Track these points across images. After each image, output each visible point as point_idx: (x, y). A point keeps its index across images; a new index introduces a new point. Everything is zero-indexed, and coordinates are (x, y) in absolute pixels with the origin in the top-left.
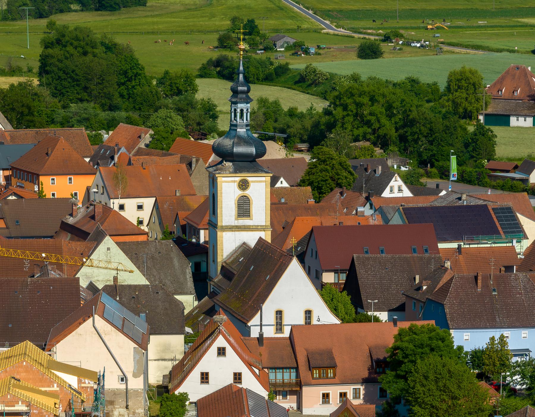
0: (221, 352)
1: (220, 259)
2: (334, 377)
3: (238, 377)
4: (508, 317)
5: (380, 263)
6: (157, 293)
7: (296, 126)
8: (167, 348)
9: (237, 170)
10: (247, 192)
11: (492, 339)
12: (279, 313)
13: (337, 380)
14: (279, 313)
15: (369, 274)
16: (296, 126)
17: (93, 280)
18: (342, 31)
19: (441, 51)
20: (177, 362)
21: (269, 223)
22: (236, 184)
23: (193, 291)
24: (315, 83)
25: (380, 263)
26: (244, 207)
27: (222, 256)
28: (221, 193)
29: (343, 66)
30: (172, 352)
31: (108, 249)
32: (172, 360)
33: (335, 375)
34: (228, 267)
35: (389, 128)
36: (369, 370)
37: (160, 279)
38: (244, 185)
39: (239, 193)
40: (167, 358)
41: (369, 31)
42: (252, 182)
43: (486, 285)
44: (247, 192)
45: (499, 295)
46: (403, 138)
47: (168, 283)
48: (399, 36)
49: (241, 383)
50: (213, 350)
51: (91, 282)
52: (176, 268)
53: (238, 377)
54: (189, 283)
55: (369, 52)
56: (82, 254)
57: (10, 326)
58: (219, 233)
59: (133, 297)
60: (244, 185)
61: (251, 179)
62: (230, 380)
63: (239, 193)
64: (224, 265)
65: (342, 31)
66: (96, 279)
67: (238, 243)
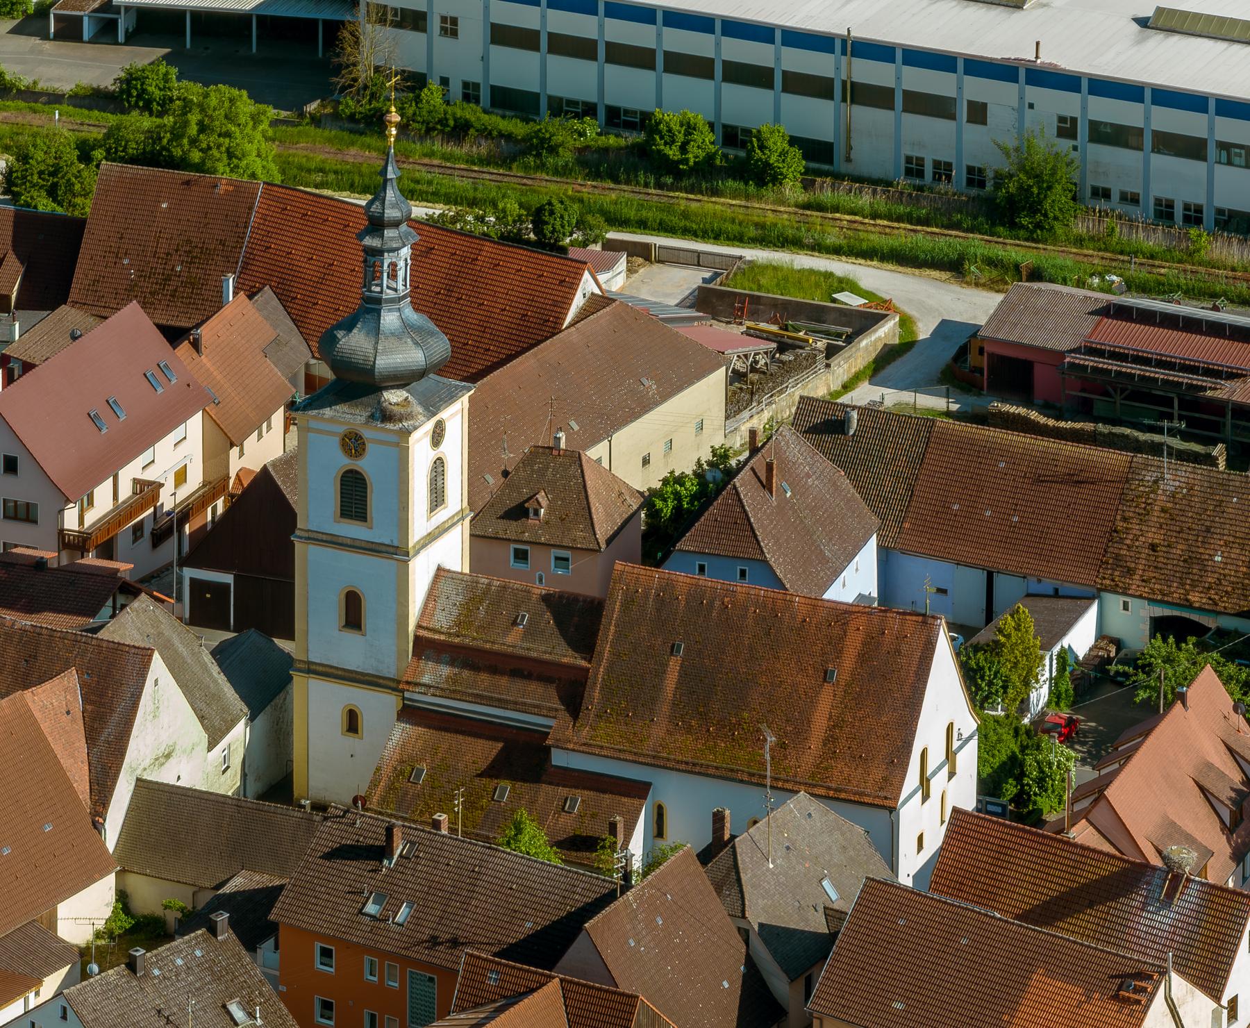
6: (810, 815)
34: (457, 640)
56: (68, 713)
59: (788, 848)
64: (422, 633)
66: (141, 767)
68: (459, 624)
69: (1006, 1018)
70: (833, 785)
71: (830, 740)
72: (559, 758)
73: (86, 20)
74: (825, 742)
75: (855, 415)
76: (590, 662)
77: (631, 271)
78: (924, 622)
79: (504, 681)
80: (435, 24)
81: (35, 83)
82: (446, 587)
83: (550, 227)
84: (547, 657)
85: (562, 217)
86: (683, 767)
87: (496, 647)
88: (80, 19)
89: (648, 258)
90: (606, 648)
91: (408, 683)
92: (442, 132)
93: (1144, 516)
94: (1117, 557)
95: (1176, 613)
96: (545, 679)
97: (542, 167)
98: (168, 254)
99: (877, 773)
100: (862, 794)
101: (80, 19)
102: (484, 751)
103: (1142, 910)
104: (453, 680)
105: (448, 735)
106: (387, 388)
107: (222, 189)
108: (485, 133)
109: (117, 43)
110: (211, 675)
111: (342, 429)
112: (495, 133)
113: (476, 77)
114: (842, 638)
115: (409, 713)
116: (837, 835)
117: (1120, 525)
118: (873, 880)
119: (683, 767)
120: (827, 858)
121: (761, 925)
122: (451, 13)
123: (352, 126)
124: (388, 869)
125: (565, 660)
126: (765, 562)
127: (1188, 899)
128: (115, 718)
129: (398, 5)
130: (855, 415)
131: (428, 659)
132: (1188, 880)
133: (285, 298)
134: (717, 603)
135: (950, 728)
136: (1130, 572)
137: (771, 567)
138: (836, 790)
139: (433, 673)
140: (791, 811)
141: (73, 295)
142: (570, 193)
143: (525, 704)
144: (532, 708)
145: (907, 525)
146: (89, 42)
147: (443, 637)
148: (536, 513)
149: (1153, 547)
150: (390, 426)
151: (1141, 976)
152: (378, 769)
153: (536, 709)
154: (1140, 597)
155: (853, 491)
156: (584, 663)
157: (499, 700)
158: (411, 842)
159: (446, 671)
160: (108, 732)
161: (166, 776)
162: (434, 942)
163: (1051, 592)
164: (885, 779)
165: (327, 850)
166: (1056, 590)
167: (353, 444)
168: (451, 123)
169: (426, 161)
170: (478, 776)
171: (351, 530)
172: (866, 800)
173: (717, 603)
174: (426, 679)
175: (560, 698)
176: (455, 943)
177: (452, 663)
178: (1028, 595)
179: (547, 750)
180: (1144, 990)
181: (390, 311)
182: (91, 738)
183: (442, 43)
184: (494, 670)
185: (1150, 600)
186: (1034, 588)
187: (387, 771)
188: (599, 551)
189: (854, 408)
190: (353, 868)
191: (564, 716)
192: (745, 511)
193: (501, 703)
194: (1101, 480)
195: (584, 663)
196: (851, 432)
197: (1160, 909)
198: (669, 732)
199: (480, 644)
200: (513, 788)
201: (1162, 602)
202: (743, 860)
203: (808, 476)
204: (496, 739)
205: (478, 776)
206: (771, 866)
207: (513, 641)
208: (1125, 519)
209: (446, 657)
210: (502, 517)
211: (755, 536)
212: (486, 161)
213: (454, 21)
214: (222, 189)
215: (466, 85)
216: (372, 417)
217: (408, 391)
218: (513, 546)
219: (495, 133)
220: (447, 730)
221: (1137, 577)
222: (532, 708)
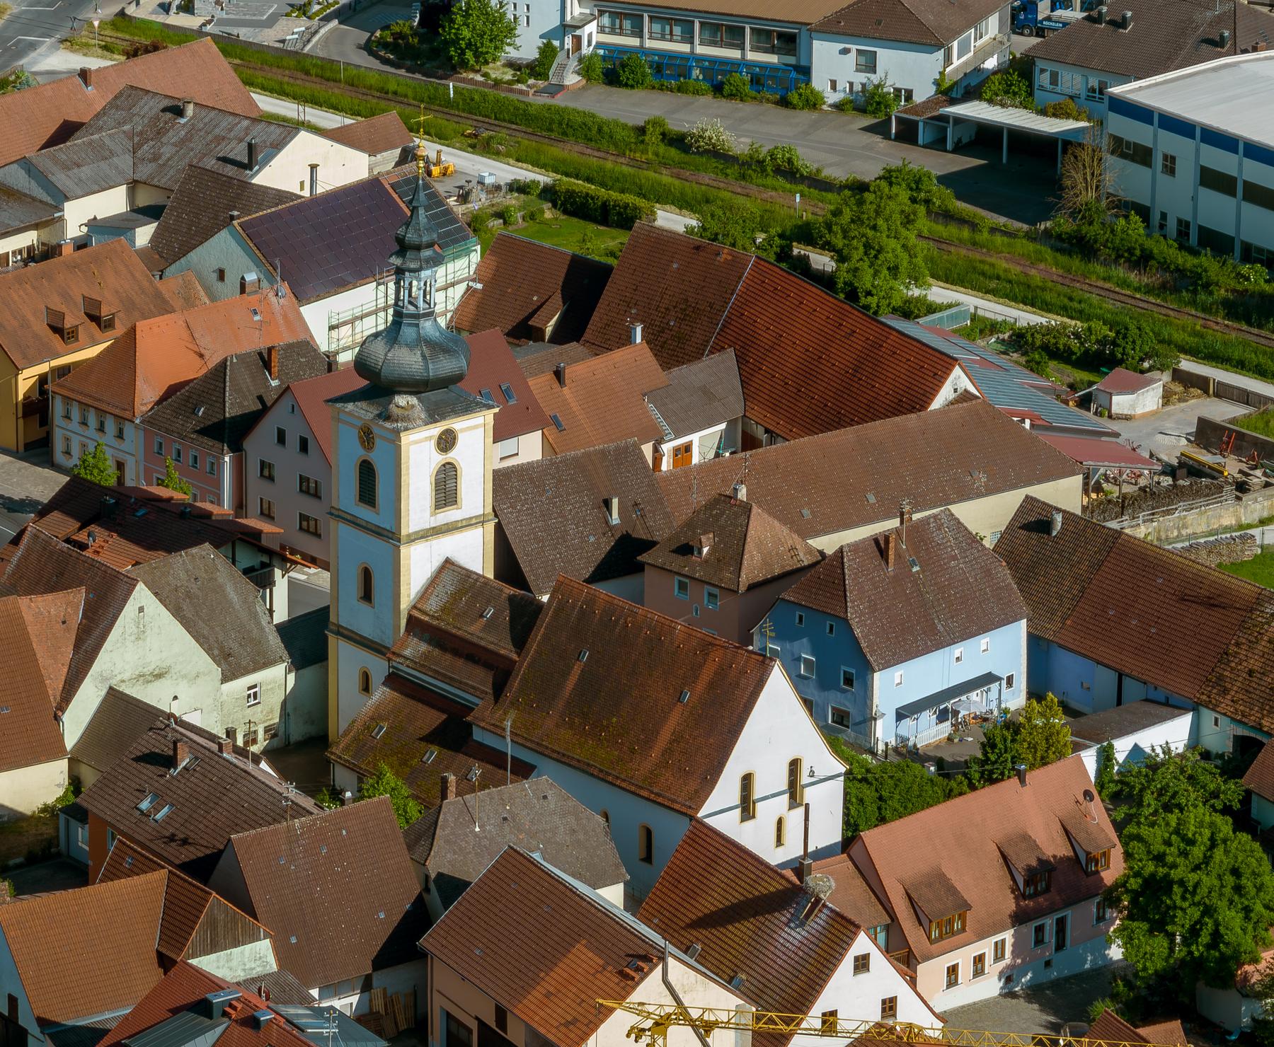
0: (862, 964)
1: (405, 604)
2: (963, 929)
3: (889, 1006)
4: (952, 617)
5: (531, 479)
6: (545, 797)
10: (452, 456)
12: (747, 781)
13: (969, 933)
14: (747, 781)
15: (519, 511)
17: (113, 682)
21: (489, 509)
22: (433, 443)
23: (285, 655)
25: (531, 479)
26: (446, 488)
27: (409, 596)
28: (408, 468)
31: (141, 609)
34: (435, 623)
36: (1013, 892)
37: (217, 641)
38: (447, 442)
39: (438, 459)
42: (463, 430)
45: (923, 571)
49: (894, 1016)
50: (847, 963)
51: (111, 688)
52: (237, 607)
53: (889, 1006)
54: (271, 637)
56: (64, 622)
57: (294, 940)
59: (505, 819)
60: (447, 442)
61: (457, 424)
62: (876, 1016)
63: (438, 459)
64: (416, 614)
66: (119, 678)
67: (437, 563)
68: (443, 610)
69: (542, 975)
70: (656, 790)
71: (667, 752)
72: (478, 735)
73: (921, 125)
74: (664, 752)
75: (1059, 518)
76: (519, 655)
77: (1167, 398)
78: (763, 662)
79: (460, 662)
80: (1158, 161)
81: (818, 171)
82: (447, 577)
83: (1121, 350)
84: (492, 647)
85: (1134, 342)
86: (555, 755)
87: (459, 633)
88: (916, 123)
89: (1206, 392)
90: (533, 646)
91: (394, 653)
92: (1128, 260)
93: (1252, 644)
94: (1221, 678)
95: (1253, 735)
96: (488, 666)
97: (1193, 303)
98: (667, 309)
99: (693, 785)
100: (673, 801)
101: (916, 123)
102: (432, 719)
103: (787, 925)
104: (426, 656)
105: (412, 702)
106: (400, 393)
107: (722, 258)
108: (1164, 266)
109: (946, 151)
110: (258, 623)
111: (359, 424)
112: (1172, 267)
113: (1187, 217)
114: (701, 666)
115: (394, 680)
116: (571, 819)
117: (1233, 649)
118: (515, 851)
119: (555, 755)
120: (548, 835)
121: (440, 875)
122: (1171, 152)
123: (1059, 244)
124: (172, 776)
125: (502, 652)
126: (846, 620)
127: (821, 919)
128: (97, 632)
129: (1132, 140)
130: (1059, 518)
131: (415, 636)
132: (824, 906)
133: (741, 360)
134: (622, 621)
135: (795, 765)
136: (1225, 691)
137: (850, 626)
138: (657, 794)
139: (415, 648)
140: (525, 790)
141: (588, 335)
142: (1198, 327)
143: (467, 684)
144: (470, 685)
145: (1068, 622)
146: (924, 146)
147: (427, 619)
148: (700, 552)
149: (1251, 673)
150: (388, 425)
151: (646, 959)
152: (354, 722)
153: (474, 690)
154: (1225, 714)
155: (1010, 580)
156: (515, 657)
157: (451, 678)
158: (197, 758)
159: (423, 647)
160: (90, 642)
161: (156, 696)
162: (172, 838)
163: (1163, 700)
164: (696, 791)
165: (139, 754)
166: (1167, 699)
167: (367, 437)
168: (1138, 252)
169: (1100, 283)
170: (421, 739)
171: (364, 513)
172: (677, 807)
173: (622, 621)
174: (407, 652)
175: (494, 684)
176: (185, 842)
177: (429, 642)
178: (1146, 700)
179: (469, 726)
180: (642, 970)
181: (410, 325)
182: (77, 647)
183: (1163, 179)
184: (456, 653)
185: (1233, 719)
186: (1153, 695)
187: (358, 725)
188: (737, 592)
189: (1058, 510)
190: (149, 770)
191: (491, 698)
192: (844, 574)
193: (450, 681)
194: (1231, 606)
195: (515, 657)
196: (1054, 534)
197: (797, 926)
198: (557, 726)
199: (449, 628)
200: (439, 753)
201: (1240, 722)
202: (446, 820)
203: (954, 558)
204: (442, 710)
205: (421, 739)
206: (477, 829)
207: (473, 631)
208: (1238, 644)
209: (427, 635)
210: (673, 551)
211: (845, 596)
212: (1149, 290)
213: (1173, 159)
214: (722, 258)
215: (1180, 221)
216: (379, 416)
217: (419, 399)
218: (677, 578)
219: (1172, 267)
220: (413, 698)
221: (1229, 697)
222: (470, 685)
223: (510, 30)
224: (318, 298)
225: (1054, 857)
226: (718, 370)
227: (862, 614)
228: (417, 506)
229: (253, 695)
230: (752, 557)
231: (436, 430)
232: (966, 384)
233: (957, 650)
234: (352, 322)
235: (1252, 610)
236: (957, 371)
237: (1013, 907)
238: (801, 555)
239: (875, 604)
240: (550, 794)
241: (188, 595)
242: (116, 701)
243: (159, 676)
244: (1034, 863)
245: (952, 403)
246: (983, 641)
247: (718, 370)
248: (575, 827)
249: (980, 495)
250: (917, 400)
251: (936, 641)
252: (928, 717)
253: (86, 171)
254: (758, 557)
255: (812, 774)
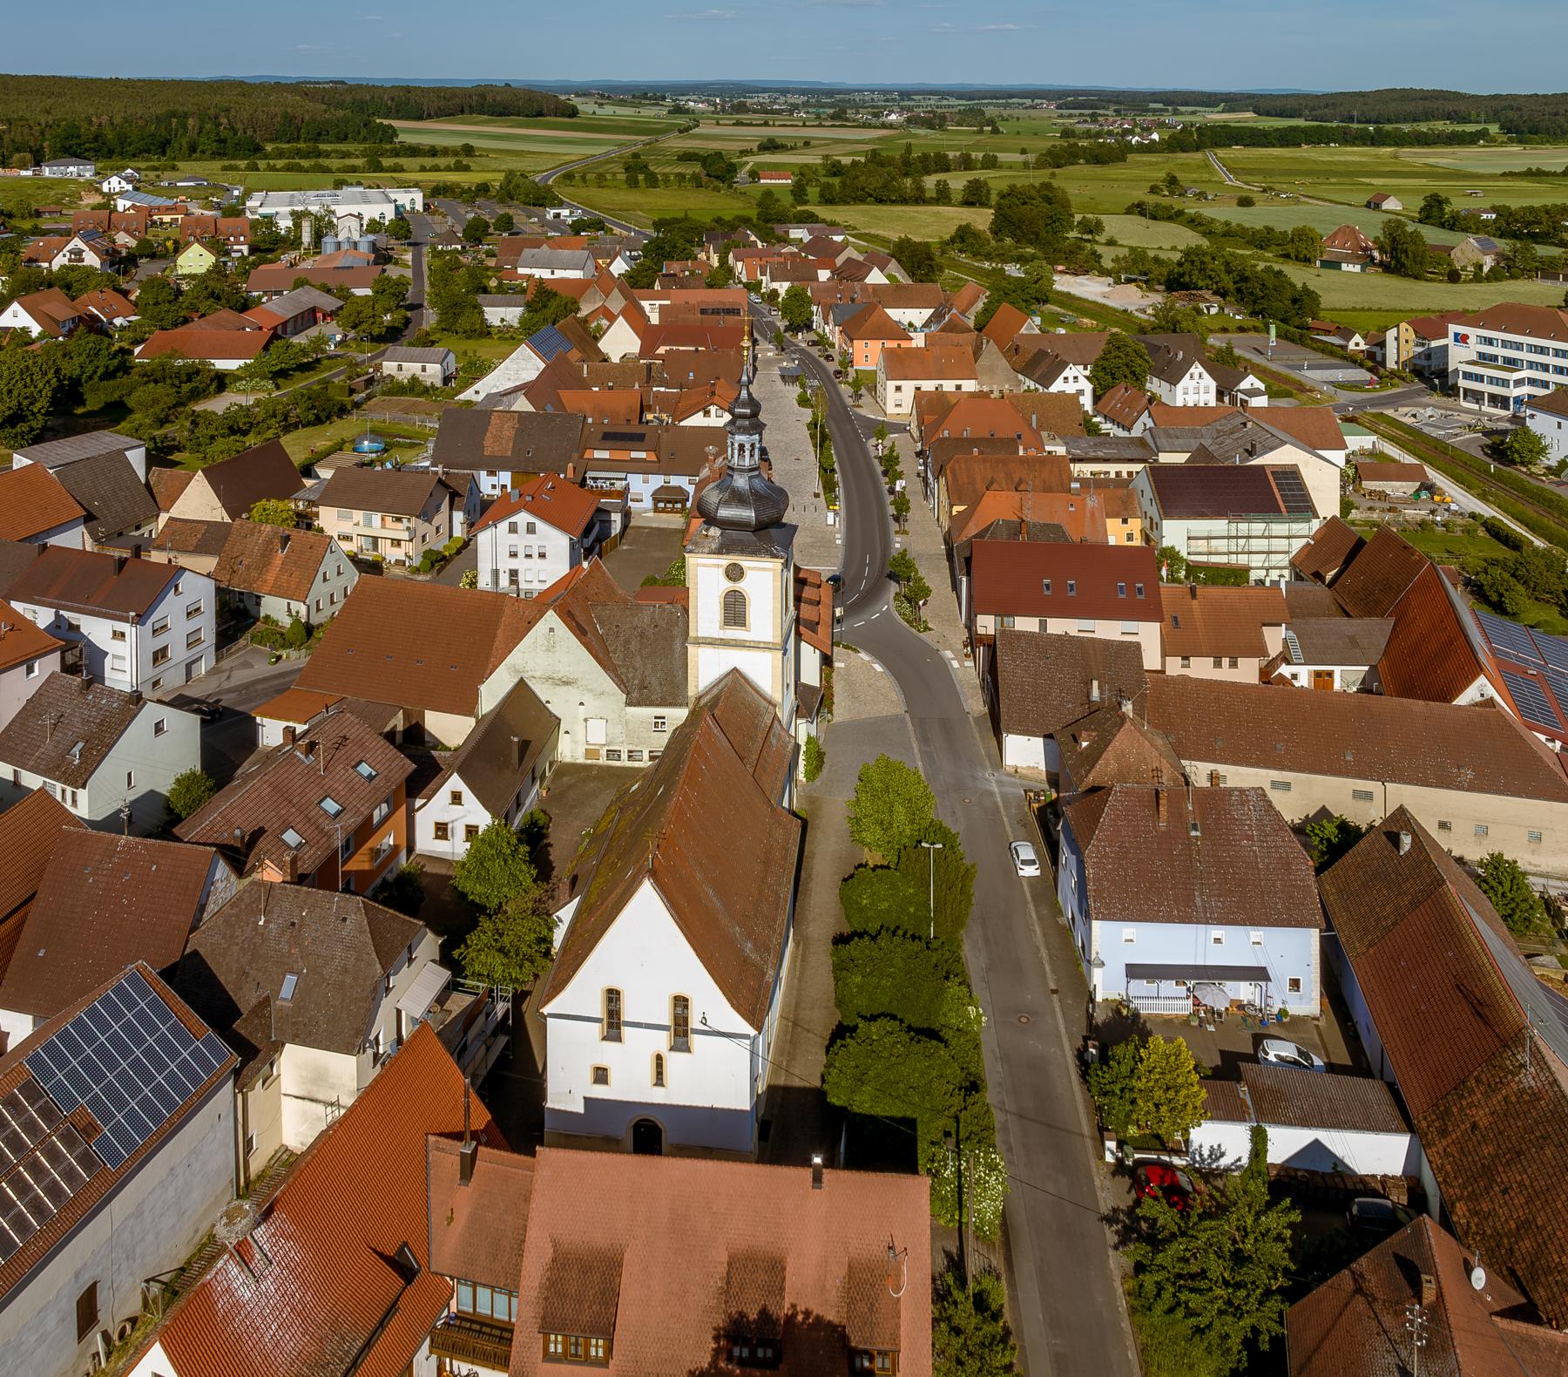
4: (1220, 896)
5: (1037, 645)
6: (344, 920)
7: (1156, 271)
8: (319, 1077)
9: (723, 549)
10: (740, 586)
11: (1234, 665)
12: (613, 996)
16: (1156, 271)
17: (525, 675)
18: (1239, 184)
19: (1298, 202)
20: (343, 1112)
22: (721, 572)
24: (1200, 224)
26: (735, 609)
29: (1223, 213)
30: (332, 1087)
31: (552, 630)
32: (332, 1104)
33: (609, 1350)
35: (1228, 282)
38: (735, 573)
40: (321, 1097)
41: (1406, 128)
43: (1177, 815)
44: (740, 586)
45: (1203, 838)
46: (1239, 290)
47: (655, 682)
48: (1271, 189)
51: (522, 680)
55: (1245, 202)
58: (691, 649)
59: (293, 924)
60: (735, 573)
65: (1239, 184)
94: (1448, 1111)
117: (1472, 1083)
121: (195, 953)
135: (681, 1003)
136: (1443, 1133)
208: (1477, 1080)
223: (1543, 451)
224: (1180, 518)
225: (807, 1313)
226: (1376, 631)
227: (1106, 856)
228: (706, 614)
229: (659, 722)
230: (1107, 765)
231: (725, 561)
232: (1491, 692)
233: (1217, 931)
234: (1209, 538)
235: (1506, 1046)
236: (1482, 680)
237: (704, 1361)
238: (1164, 779)
239: (1128, 852)
240: (352, 918)
241: (642, 635)
242: (522, 689)
243: (567, 683)
244: (753, 1316)
245: (1477, 704)
246: (1256, 933)
247: (1376, 631)
248: (350, 967)
249: (1459, 788)
250: (1447, 694)
251: (1184, 913)
252: (1169, 987)
253: (1176, 442)
254: (1113, 765)
255: (704, 1021)
